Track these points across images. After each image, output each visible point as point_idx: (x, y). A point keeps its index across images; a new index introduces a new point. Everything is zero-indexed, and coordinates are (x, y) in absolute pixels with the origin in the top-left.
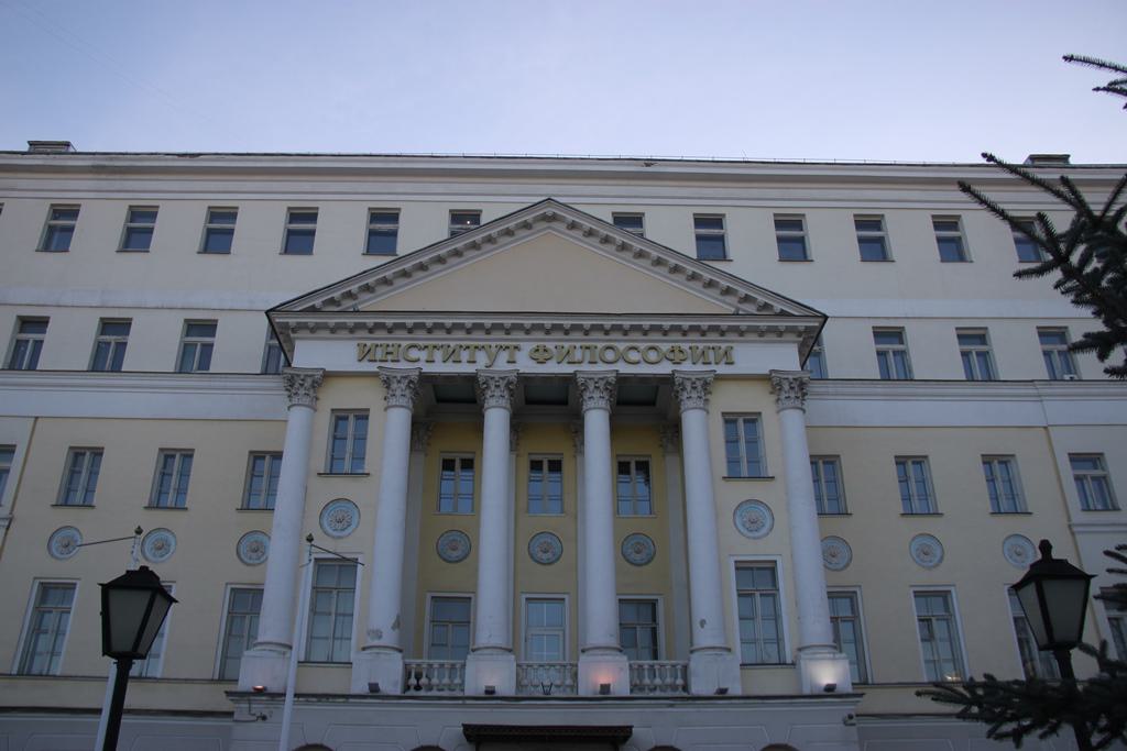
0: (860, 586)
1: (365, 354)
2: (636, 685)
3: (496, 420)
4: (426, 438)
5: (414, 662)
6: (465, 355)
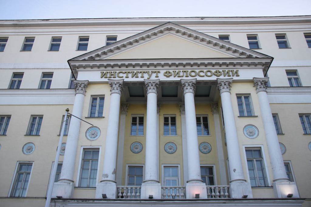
0: (290, 161)
1: (103, 75)
2: (209, 195)
3: (152, 98)
4: (126, 109)
5: (121, 186)
6: (140, 75)
